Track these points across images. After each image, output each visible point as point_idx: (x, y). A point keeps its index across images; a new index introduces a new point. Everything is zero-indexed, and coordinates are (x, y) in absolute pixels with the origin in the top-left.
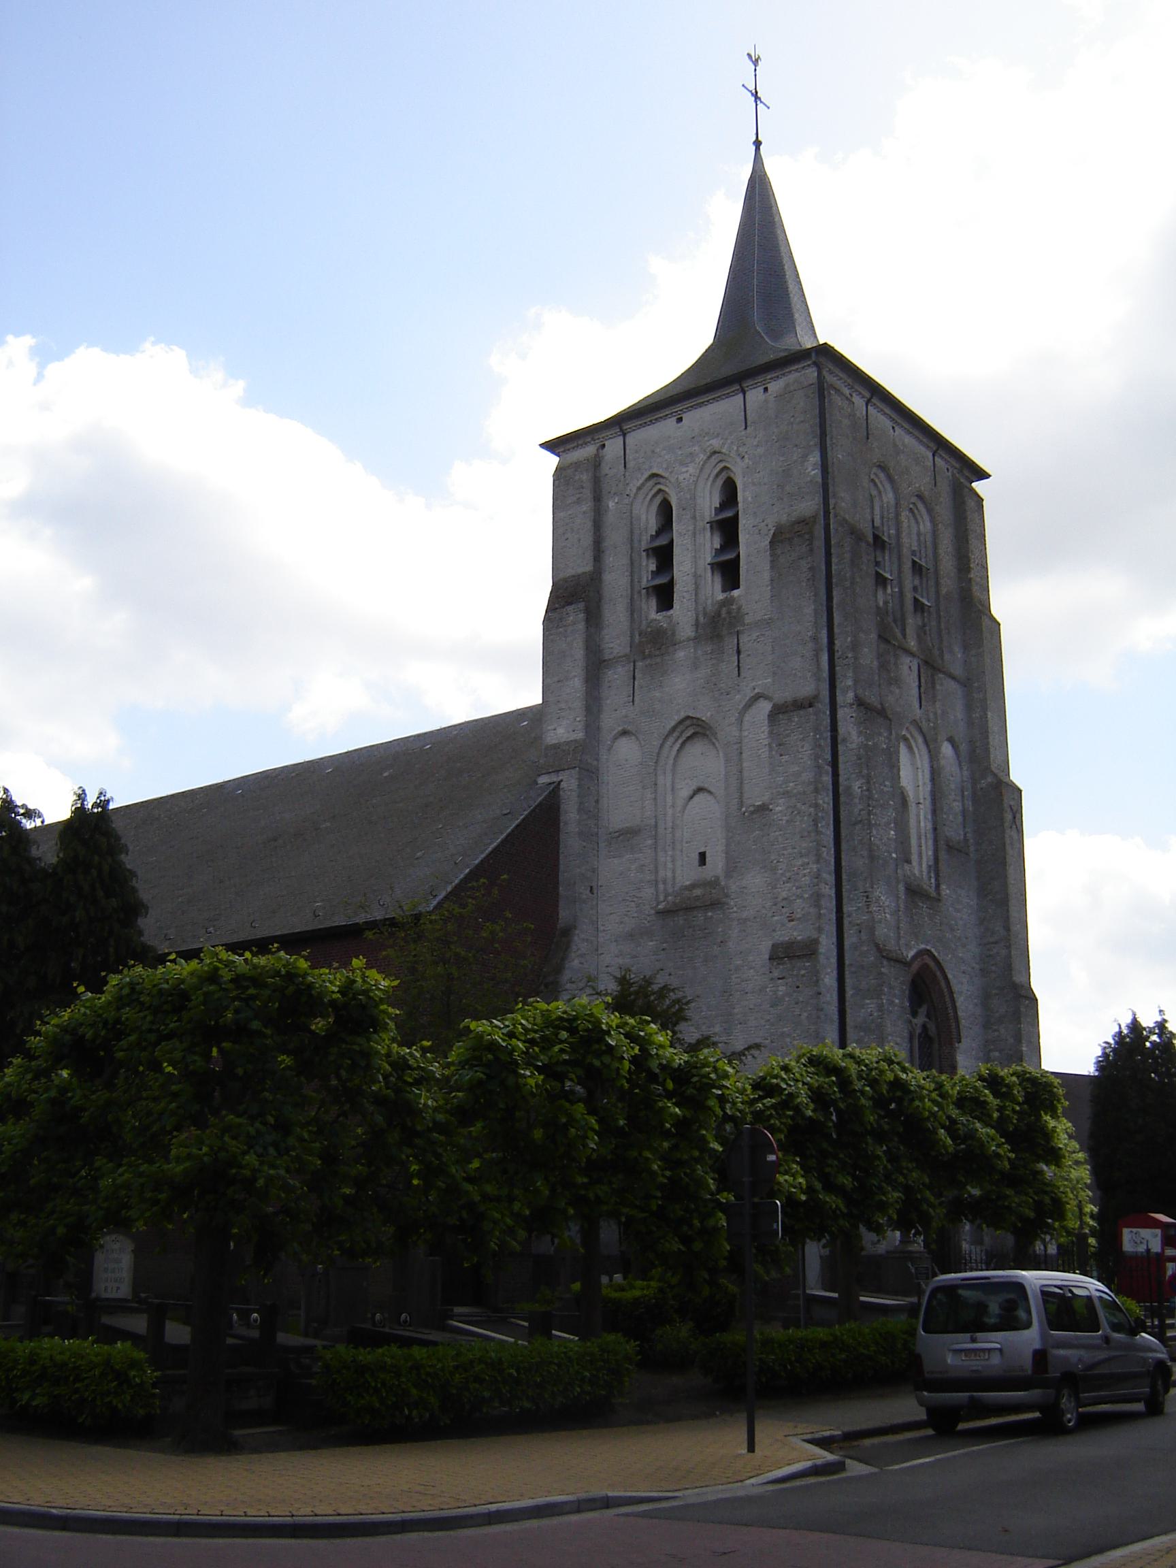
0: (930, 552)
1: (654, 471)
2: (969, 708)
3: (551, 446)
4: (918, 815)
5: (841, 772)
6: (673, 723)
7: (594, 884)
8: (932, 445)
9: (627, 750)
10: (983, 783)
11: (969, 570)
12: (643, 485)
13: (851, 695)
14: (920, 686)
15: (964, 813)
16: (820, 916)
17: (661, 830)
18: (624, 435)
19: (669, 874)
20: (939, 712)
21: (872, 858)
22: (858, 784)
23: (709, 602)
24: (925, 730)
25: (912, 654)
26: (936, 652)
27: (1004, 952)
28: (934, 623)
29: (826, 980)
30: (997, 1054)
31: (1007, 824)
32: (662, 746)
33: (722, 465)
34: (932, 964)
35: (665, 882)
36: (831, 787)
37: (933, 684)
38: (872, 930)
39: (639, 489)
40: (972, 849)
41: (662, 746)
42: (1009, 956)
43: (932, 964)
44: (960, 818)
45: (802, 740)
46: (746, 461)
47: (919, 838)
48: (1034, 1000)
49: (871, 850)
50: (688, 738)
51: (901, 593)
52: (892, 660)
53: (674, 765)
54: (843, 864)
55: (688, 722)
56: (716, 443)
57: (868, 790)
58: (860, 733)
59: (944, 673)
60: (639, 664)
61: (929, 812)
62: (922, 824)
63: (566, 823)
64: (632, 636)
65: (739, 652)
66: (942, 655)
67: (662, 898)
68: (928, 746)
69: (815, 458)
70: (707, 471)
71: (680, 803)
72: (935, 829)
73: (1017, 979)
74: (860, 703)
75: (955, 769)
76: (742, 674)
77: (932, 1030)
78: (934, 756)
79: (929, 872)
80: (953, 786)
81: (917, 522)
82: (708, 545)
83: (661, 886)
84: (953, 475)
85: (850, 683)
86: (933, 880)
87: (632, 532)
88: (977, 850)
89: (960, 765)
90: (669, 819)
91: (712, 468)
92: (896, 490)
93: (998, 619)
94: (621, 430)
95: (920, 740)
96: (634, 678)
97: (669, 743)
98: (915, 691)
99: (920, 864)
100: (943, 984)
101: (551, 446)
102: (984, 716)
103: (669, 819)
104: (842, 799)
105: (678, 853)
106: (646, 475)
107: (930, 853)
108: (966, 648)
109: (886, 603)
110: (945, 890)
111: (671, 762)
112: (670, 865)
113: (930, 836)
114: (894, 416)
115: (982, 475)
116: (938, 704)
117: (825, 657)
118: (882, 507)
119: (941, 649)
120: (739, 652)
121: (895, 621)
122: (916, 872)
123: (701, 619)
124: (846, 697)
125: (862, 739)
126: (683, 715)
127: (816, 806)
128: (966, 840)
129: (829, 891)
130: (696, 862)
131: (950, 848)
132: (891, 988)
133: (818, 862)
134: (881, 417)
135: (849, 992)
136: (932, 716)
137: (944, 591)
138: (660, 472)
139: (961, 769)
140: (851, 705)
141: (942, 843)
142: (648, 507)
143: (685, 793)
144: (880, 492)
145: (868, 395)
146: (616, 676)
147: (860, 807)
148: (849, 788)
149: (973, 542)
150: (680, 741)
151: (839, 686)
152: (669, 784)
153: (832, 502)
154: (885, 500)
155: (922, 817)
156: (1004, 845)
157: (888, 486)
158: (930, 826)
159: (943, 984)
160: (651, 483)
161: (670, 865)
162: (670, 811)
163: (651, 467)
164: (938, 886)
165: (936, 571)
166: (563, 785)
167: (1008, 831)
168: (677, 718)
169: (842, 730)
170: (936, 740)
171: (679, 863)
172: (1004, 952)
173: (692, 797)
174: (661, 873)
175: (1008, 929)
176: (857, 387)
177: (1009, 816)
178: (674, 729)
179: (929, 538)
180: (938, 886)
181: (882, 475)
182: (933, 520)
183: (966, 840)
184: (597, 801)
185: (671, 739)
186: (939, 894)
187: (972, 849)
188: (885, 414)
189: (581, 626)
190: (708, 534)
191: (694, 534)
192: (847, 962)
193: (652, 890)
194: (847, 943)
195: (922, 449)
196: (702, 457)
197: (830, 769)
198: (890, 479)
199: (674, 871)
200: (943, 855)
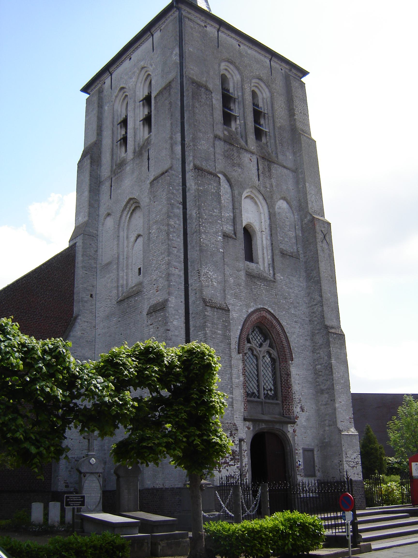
0: (270, 108)
1: (121, 86)
2: (297, 183)
3: (85, 90)
4: (262, 238)
5: (188, 207)
6: (125, 203)
7: (94, 293)
8: (267, 55)
9: (110, 223)
10: (306, 221)
11: (294, 115)
12: (118, 94)
13: (192, 165)
14: (258, 170)
15: (296, 237)
16: (169, 286)
17: (121, 260)
18: (111, 75)
19: (125, 282)
20: (274, 184)
21: (201, 251)
22: (195, 211)
23: (141, 140)
24: (263, 192)
25: (253, 153)
26: (274, 155)
27: (320, 309)
28: (273, 141)
29: (175, 323)
30: (319, 366)
31: (318, 240)
32: (121, 216)
33: (146, 74)
34: (269, 316)
35: (122, 286)
36: (182, 216)
37: (270, 170)
38: (201, 291)
39: (116, 97)
40: (302, 256)
41: (121, 216)
42: (323, 311)
43: (269, 316)
44: (294, 241)
45: (163, 191)
46: (153, 66)
47: (263, 250)
48: (341, 336)
49: (200, 246)
50: (133, 210)
51: (245, 124)
52: (236, 154)
53: (128, 225)
54: (189, 257)
55: (132, 202)
56: (142, 64)
57: (199, 213)
58: (196, 184)
59: (277, 164)
60: (113, 179)
61: (269, 235)
62: (264, 242)
63: (78, 263)
64: (112, 167)
65: (148, 159)
66: (277, 157)
67: (120, 295)
68: (266, 200)
69: (177, 50)
70: (140, 78)
71: (131, 244)
72: (272, 244)
73: (328, 323)
74: (197, 168)
75: (290, 215)
76: (150, 170)
77: (274, 353)
78: (271, 206)
79: (269, 267)
80: (288, 223)
81: (262, 93)
82: (141, 113)
83: (120, 289)
84: (285, 72)
85: (191, 158)
86: (271, 272)
87: (113, 118)
88: (304, 256)
89: (293, 213)
90: (125, 253)
91: (143, 76)
92: (241, 73)
93: (315, 139)
94: (110, 73)
95: (261, 198)
96: (111, 186)
97: (125, 214)
98: (255, 171)
99: (264, 264)
100: (278, 327)
101: (85, 90)
102: (304, 187)
103: (125, 253)
104: (188, 221)
105: (130, 271)
106: (118, 89)
107: (269, 257)
108: (294, 153)
109: (236, 129)
110: (279, 276)
111: (127, 223)
112: (125, 277)
113: (270, 248)
114: (238, 38)
115: (305, 73)
116: (273, 180)
117: (178, 149)
118: (234, 83)
119: (276, 154)
120: (148, 159)
121: (242, 137)
122: (262, 269)
123: (137, 149)
124: (189, 167)
125: (196, 187)
126: (128, 198)
127: (168, 225)
128: (298, 251)
129: (178, 272)
130: (137, 274)
131: (283, 254)
132: (213, 323)
133: (168, 256)
134: (229, 39)
135: (192, 329)
136: (268, 186)
137: (278, 125)
138: (124, 86)
139: (294, 215)
140: (192, 170)
141: (277, 252)
142: (122, 105)
143: (132, 239)
144: (232, 76)
145: (218, 26)
146: (105, 188)
147: (196, 224)
148: (191, 215)
149: (297, 102)
150: (130, 213)
151: (187, 161)
152: (125, 237)
153: (184, 70)
154: (235, 79)
155: (264, 239)
156: (317, 250)
157: (236, 72)
158: (269, 243)
159: (278, 327)
160: (122, 93)
161: (125, 277)
162: (126, 249)
163: (120, 85)
164: (274, 274)
165: (273, 116)
166: (77, 244)
167: (319, 244)
168: (126, 200)
169: (188, 185)
170: (272, 198)
171: (130, 275)
172: (320, 309)
173: (136, 241)
174: (121, 282)
175: (321, 296)
176: (208, 21)
177: (320, 236)
178: (126, 206)
179: (269, 100)
180: (274, 274)
181: (231, 67)
182: (270, 92)
183: (298, 251)
184: (96, 251)
185: (125, 213)
186: (275, 279)
187: (302, 256)
188: (231, 37)
189: (89, 166)
190: (142, 108)
191: (134, 109)
192: (191, 312)
193: (116, 291)
194: (190, 301)
195: (262, 58)
196: (137, 72)
197: (181, 206)
198: (238, 69)
199: (127, 280)
200: (278, 258)
